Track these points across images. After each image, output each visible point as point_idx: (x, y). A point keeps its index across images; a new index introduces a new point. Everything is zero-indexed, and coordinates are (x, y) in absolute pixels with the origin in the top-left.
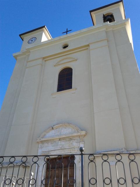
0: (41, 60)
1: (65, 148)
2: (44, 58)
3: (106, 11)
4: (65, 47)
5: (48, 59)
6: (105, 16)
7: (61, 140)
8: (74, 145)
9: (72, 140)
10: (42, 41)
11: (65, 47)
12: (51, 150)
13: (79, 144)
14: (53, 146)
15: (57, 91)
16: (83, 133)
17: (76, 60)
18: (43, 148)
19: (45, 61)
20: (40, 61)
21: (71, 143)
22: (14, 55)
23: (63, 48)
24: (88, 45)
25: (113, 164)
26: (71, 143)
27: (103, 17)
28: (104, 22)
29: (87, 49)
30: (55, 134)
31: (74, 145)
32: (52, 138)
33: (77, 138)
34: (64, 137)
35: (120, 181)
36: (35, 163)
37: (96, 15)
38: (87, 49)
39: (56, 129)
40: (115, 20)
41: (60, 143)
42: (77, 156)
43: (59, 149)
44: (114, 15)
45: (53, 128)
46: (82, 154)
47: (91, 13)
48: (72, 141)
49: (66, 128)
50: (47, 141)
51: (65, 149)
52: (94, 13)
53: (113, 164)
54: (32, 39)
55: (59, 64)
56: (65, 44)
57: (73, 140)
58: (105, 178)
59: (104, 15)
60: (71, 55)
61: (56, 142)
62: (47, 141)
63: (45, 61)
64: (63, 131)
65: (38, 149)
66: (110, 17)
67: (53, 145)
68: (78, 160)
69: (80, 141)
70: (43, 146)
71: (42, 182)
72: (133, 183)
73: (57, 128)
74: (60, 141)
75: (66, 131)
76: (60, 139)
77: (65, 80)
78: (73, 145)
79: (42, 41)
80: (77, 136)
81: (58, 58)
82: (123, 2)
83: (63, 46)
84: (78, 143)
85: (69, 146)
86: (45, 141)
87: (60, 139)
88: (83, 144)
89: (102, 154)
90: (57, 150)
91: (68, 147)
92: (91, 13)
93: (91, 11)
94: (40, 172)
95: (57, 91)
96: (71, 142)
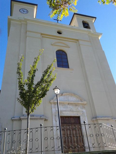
0: (40, 35)
1: (74, 110)
2: (42, 34)
3: (86, 20)
4: (59, 33)
5: (45, 36)
9: (77, 106)
14: (64, 108)
20: (39, 35)
21: (77, 108)
22: (9, 18)
23: (57, 32)
26: (77, 108)
27: (104, 51)
29: (76, 42)
30: (64, 99)
31: (80, 110)
32: (63, 102)
33: (80, 105)
38: (76, 42)
39: (64, 96)
40: (102, 33)
41: (69, 106)
46: (85, 125)
49: (71, 97)
52: (76, 16)
54: (25, 10)
55: (55, 44)
60: (64, 41)
63: (43, 37)
64: (70, 98)
67: (63, 107)
75: (73, 99)
76: (68, 104)
79: (78, 26)
80: (80, 104)
81: (56, 40)
82: (96, 19)
87: (68, 104)
88: (85, 110)
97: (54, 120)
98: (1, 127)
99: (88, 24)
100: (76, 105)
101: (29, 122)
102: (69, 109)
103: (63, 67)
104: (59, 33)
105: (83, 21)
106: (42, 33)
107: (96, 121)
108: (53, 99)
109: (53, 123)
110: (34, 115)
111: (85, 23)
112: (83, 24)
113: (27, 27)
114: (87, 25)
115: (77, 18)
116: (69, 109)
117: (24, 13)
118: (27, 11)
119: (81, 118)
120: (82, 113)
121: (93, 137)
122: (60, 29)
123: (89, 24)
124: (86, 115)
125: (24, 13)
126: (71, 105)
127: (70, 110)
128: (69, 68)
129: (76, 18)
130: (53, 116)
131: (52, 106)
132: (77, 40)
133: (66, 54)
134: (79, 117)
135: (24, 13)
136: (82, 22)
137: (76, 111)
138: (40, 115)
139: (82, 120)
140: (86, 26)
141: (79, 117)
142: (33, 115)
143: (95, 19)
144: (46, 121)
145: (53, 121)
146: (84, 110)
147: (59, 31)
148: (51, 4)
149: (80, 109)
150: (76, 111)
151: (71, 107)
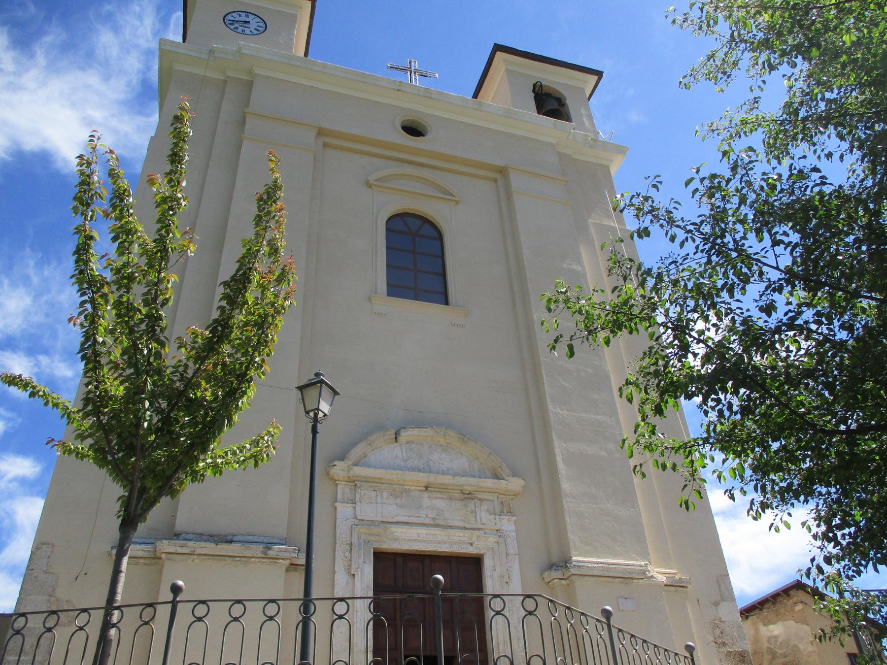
1: (451, 523)
4: (413, 130)
5: (345, 144)
7: (431, 492)
14: (401, 507)
17: (457, 203)
18: (358, 504)
19: (325, 145)
25: (719, 300)
30: (405, 461)
31: (484, 521)
38: (496, 181)
41: (426, 500)
43: (427, 521)
45: (399, 438)
47: (499, 54)
48: (472, 502)
50: (376, 484)
51: (451, 527)
52: (504, 61)
53: (719, 300)
57: (478, 503)
61: (413, 493)
62: (376, 484)
63: (325, 145)
64: (435, 457)
67: (398, 501)
72: (46, 614)
73: (412, 442)
74: (425, 494)
78: (478, 518)
84: (495, 514)
86: (367, 480)
91: (462, 524)
93: (498, 48)
96: (471, 505)
97: (340, 566)
98: (51, 596)
99: (560, 101)
100: (468, 496)
101: (309, 83)
102: (427, 516)
103: (417, 299)
104: (413, 130)
105: (535, 85)
106: (326, 125)
107: (564, 582)
108: (342, 458)
109: (333, 588)
110: (235, 539)
111: (548, 95)
112: (535, 98)
113: (250, 94)
114: (554, 105)
115: (508, 71)
116: (427, 516)
117: (247, 31)
118: (262, 24)
119: (487, 563)
120: (492, 539)
121: (505, 598)
122: (419, 109)
123: (567, 102)
124: (513, 549)
125: (243, 31)
126: (438, 495)
127: (434, 519)
128: (447, 303)
129: (504, 69)
130: (338, 546)
131: (339, 496)
132: (503, 171)
133: (437, 236)
134: (475, 563)
135: (247, 31)
136: (534, 91)
137: (465, 528)
138: (265, 541)
139: (491, 576)
140: (551, 107)
141: (475, 563)
142: (229, 538)
143: (596, 78)
144: (295, 570)
145: (334, 573)
146: (508, 525)
148: (243, 257)
149: (484, 516)
150: (465, 528)
151: (441, 504)
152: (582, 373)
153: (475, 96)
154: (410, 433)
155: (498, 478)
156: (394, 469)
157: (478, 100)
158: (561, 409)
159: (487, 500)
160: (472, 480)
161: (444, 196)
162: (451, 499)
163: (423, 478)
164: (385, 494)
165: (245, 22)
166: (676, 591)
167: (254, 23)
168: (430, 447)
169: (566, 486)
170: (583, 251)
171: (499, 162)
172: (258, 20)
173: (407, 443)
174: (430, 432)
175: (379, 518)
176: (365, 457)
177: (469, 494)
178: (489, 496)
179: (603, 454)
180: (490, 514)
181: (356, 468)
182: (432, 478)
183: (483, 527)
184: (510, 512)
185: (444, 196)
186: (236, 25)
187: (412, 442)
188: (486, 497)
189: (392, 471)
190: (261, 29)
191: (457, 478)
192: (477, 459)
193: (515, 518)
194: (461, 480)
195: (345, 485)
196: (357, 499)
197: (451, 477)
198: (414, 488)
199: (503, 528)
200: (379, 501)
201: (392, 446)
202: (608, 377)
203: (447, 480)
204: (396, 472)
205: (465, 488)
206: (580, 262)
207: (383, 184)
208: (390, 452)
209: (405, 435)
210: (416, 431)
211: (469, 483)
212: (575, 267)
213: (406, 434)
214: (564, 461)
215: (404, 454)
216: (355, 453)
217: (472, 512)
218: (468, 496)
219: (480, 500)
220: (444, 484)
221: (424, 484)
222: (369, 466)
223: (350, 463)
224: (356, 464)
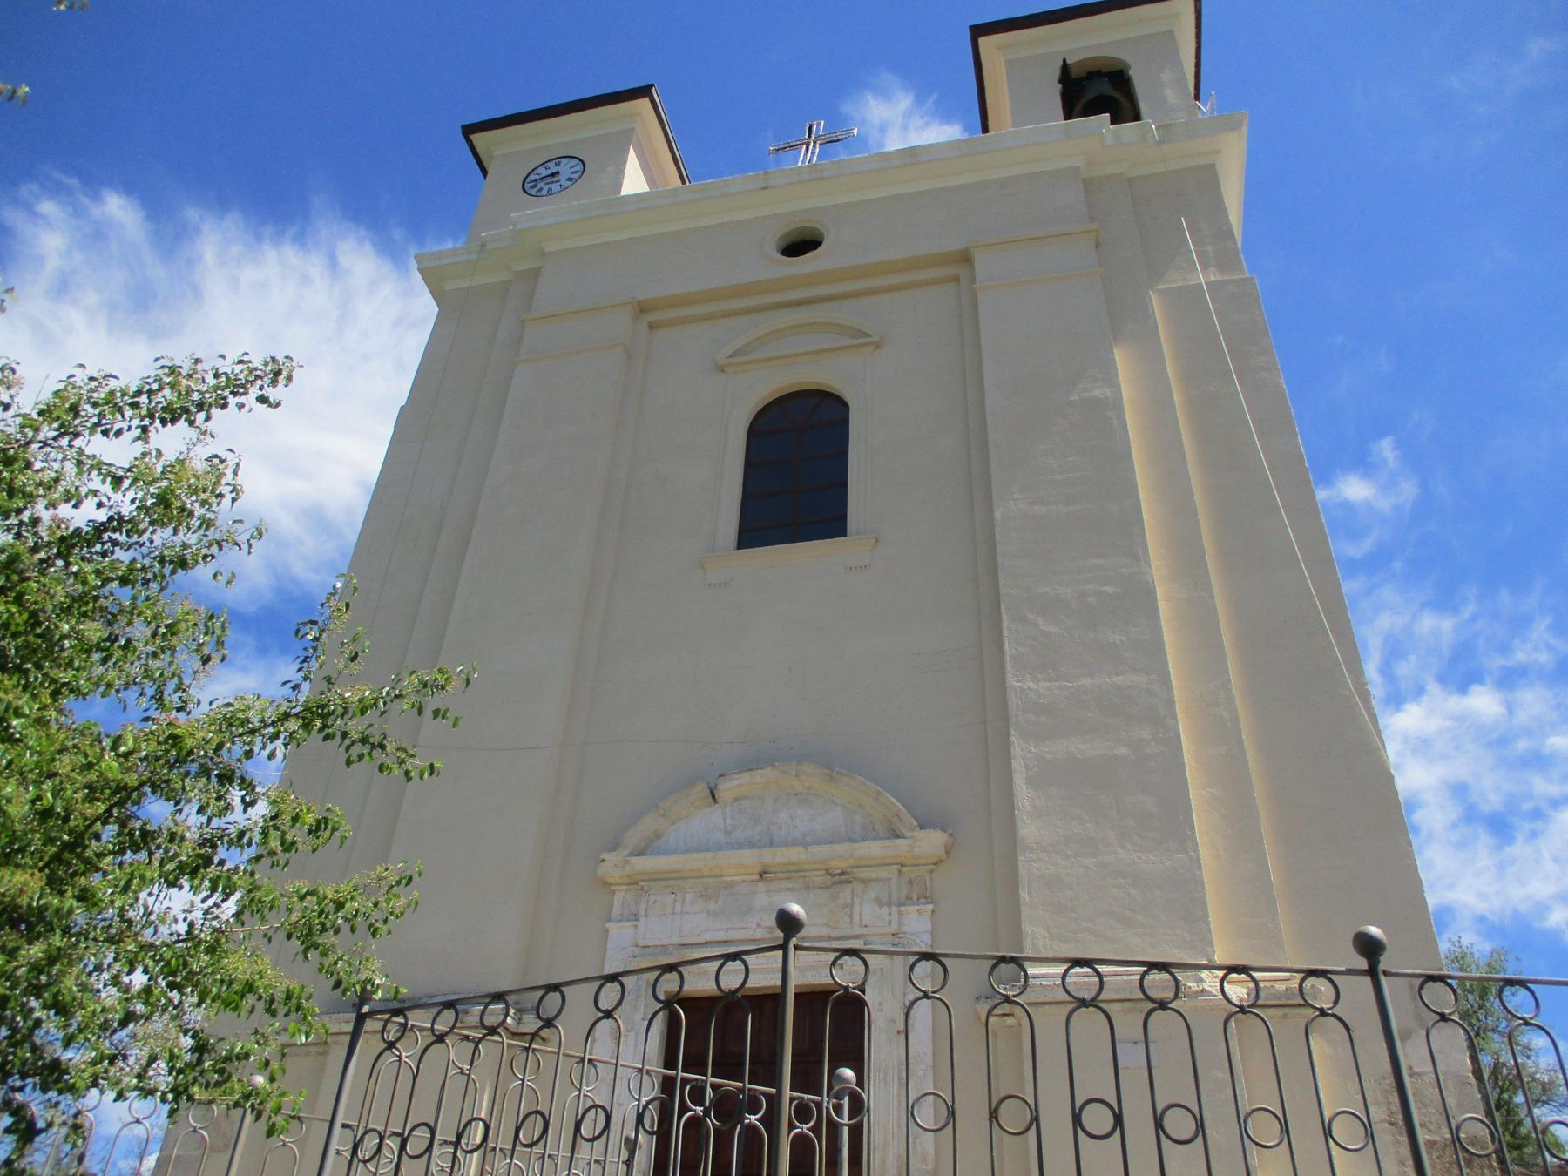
2: (642, 308)
4: (800, 245)
6: (1075, 73)
7: (772, 880)
8: (867, 920)
10: (623, 193)
11: (800, 245)
12: (702, 939)
13: (900, 913)
15: (752, 533)
16: (932, 842)
17: (877, 346)
18: (643, 920)
19: (652, 327)
24: (965, 258)
27: (1060, 81)
28: (1068, 115)
29: (957, 279)
30: (727, 832)
31: (867, 920)
34: (1006, 647)
35: (1086, 1119)
36: (608, 1014)
37: (1009, 63)
38: (957, 279)
40: (1144, 108)
42: (780, 960)
44: (1135, 73)
50: (672, 881)
52: (999, 48)
55: (748, 358)
56: (801, 230)
57: (858, 887)
58: (1002, 1094)
59: (1065, 67)
62: (672, 881)
63: (652, 327)
64: (784, 816)
65: (608, 925)
66: (1105, 88)
67: (712, 906)
68: (893, 1021)
69: (904, 893)
70: (643, 906)
71: (640, 1119)
73: (745, 797)
74: (761, 886)
77: (796, 473)
78: (856, 917)
79: (623, 193)
83: (781, 238)
84: (889, 905)
85: (828, 925)
86: (657, 877)
89: (835, 950)
90: (710, 930)
92: (984, 42)
93: (978, 31)
94: (624, 1065)
95: (752, 533)
96: (846, 893)
102: (759, 925)
118: (574, 162)
131: (616, 910)
147: (785, 236)
152: (1092, 599)
153: (985, 130)
154: (735, 783)
155: (898, 837)
156: (698, 850)
157: (992, 133)
158: (1037, 681)
159: (877, 880)
160: (842, 848)
161: (855, 342)
162: (807, 887)
163: (748, 857)
164: (689, 897)
165: (553, 175)
166: (1285, 1015)
167: (566, 168)
168: (776, 801)
169: (1028, 830)
170: (1122, 359)
171: (953, 244)
172: (564, 161)
173: (736, 800)
174: (770, 773)
175: (675, 940)
176: (659, 837)
177: (842, 874)
178: (883, 873)
179: (1122, 751)
180: (881, 904)
181: (634, 860)
182: (768, 857)
183: (864, 931)
184: (925, 897)
185: (855, 342)
186: (541, 185)
187: (745, 797)
188: (874, 876)
189: (695, 855)
190: (580, 167)
191: (814, 849)
192: (861, 806)
193: (931, 907)
194: (823, 851)
195: (627, 891)
196: (642, 912)
197: (800, 849)
198: (737, 878)
199: (905, 929)
200: (678, 909)
201: (708, 810)
202: (1151, 594)
203: (795, 854)
204: (702, 855)
205: (833, 863)
206: (1110, 379)
207: (748, 358)
208: (706, 822)
209: (726, 789)
210: (745, 778)
211: (840, 854)
212: (1097, 393)
213: (729, 785)
214: (1030, 781)
215: (728, 821)
216: (633, 838)
217: (845, 906)
218: (841, 878)
219: (864, 881)
220: (793, 864)
221: (757, 870)
222: (666, 853)
223: (626, 852)
224: (641, 853)
